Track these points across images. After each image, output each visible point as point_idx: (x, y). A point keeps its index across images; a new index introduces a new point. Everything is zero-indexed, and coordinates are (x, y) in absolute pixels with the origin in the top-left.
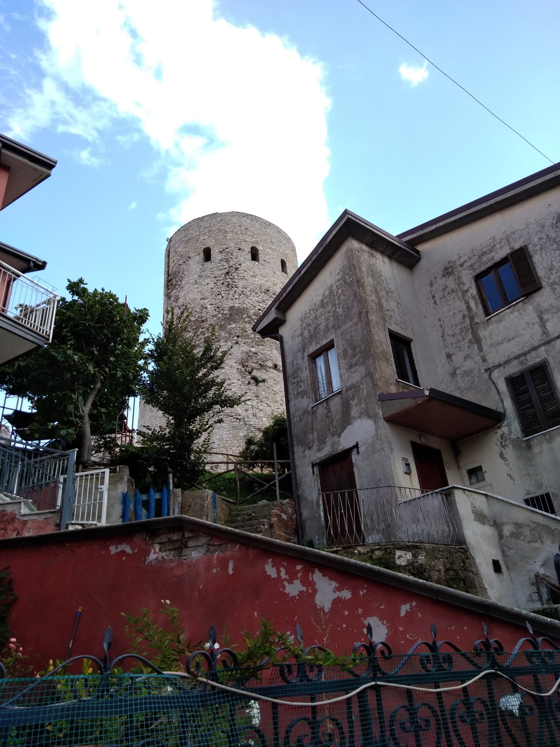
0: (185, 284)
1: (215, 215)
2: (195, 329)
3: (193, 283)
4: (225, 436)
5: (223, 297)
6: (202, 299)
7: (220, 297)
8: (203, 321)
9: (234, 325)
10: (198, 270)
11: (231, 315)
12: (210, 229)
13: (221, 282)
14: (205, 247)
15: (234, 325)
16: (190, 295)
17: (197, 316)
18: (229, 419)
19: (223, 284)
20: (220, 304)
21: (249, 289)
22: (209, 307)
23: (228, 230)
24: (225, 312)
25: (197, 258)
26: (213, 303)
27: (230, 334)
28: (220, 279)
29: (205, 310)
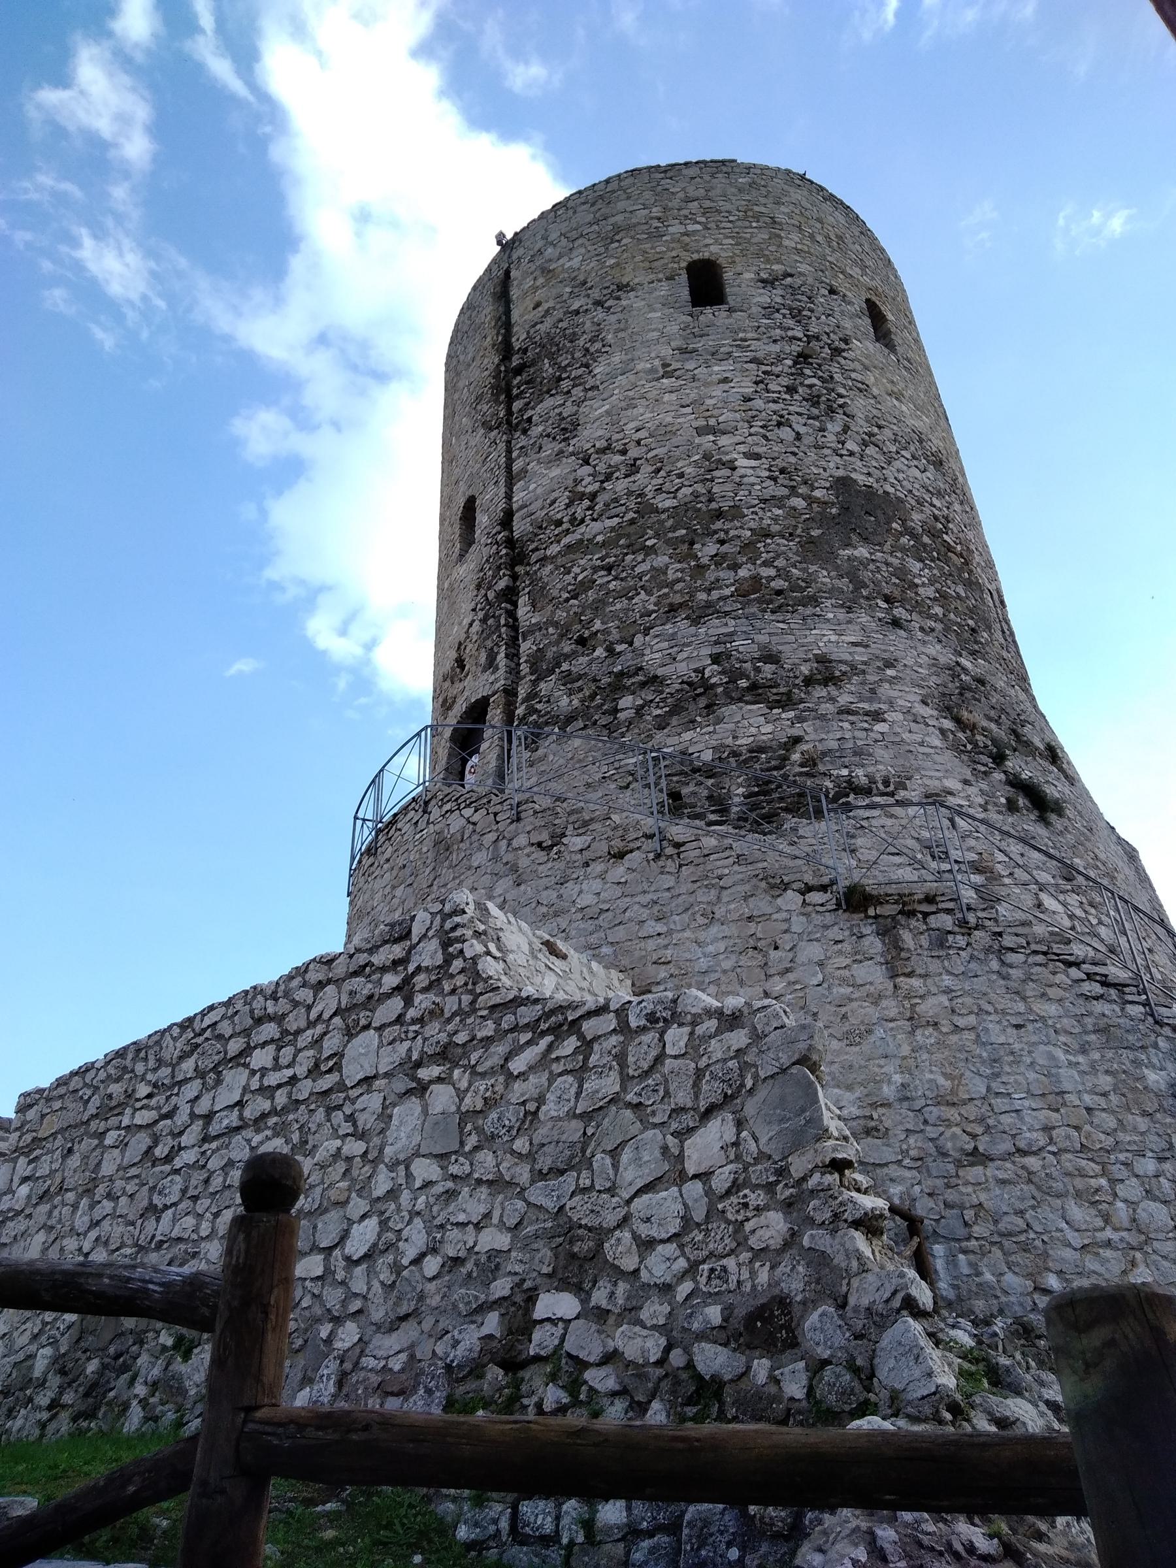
0: (611, 377)
1: (724, 166)
2: (682, 540)
3: (653, 370)
4: (1069, 1079)
5: (798, 436)
6: (700, 431)
7: (786, 433)
8: (719, 514)
9: (862, 552)
10: (673, 328)
11: (845, 509)
12: (707, 204)
13: (785, 381)
14: (696, 256)
15: (862, 552)
16: (643, 413)
17: (686, 491)
18: (1060, 978)
19: (791, 390)
20: (792, 459)
21: (887, 433)
22: (742, 462)
23: (781, 218)
24: (817, 493)
25: (664, 289)
26: (757, 449)
27: (859, 585)
28: (777, 369)
29: (726, 472)
